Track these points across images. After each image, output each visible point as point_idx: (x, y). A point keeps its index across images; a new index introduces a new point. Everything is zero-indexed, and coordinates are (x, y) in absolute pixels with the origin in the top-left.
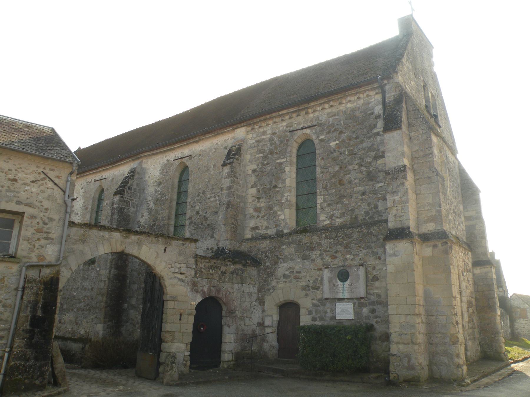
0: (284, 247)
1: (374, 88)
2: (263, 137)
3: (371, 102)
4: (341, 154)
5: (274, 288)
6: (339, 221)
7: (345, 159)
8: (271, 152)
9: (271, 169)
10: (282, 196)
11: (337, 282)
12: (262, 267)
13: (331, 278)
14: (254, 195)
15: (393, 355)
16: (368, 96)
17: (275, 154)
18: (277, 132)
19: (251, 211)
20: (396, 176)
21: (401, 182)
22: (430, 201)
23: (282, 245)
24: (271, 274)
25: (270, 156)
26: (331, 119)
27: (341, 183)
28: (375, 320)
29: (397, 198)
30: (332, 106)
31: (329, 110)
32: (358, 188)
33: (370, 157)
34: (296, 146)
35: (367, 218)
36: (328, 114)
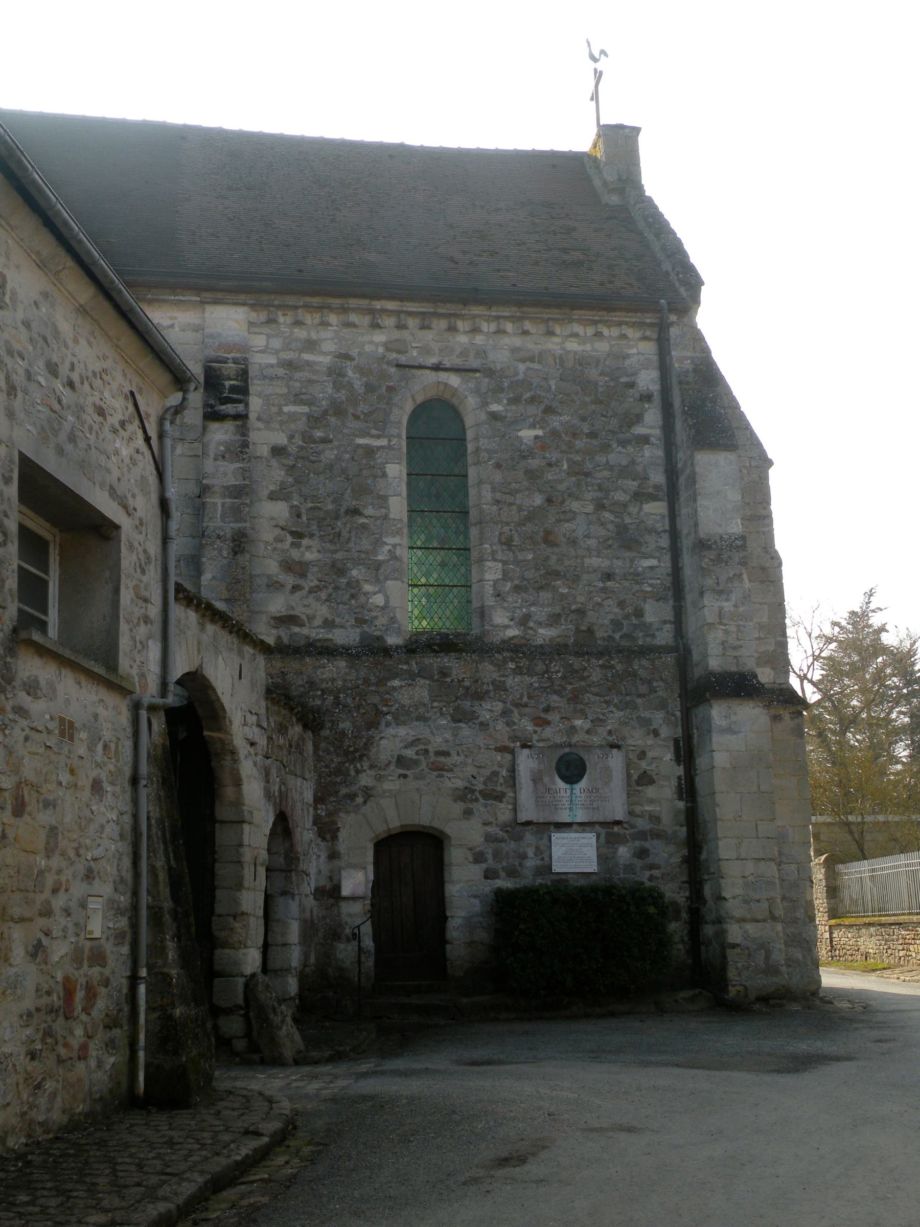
0: (396, 683)
1: (645, 323)
2: (306, 356)
3: (627, 356)
4: (550, 465)
5: (368, 793)
6: (545, 634)
7: (561, 481)
8: (338, 410)
9: (338, 458)
10: (378, 543)
11: (554, 783)
12: (326, 733)
13: (540, 771)
14: (282, 523)
15: (734, 946)
16: (623, 336)
17: (350, 418)
18: (354, 352)
19: (272, 567)
20: (725, 557)
21: (738, 572)
22: (765, 620)
23: (389, 679)
24: (356, 752)
25: (333, 420)
26: (522, 367)
27: (549, 539)
28: (647, 874)
29: (728, 606)
30: (526, 333)
31: (517, 342)
32: (594, 562)
33: (624, 491)
34: (409, 407)
35: (617, 636)
36: (514, 350)
